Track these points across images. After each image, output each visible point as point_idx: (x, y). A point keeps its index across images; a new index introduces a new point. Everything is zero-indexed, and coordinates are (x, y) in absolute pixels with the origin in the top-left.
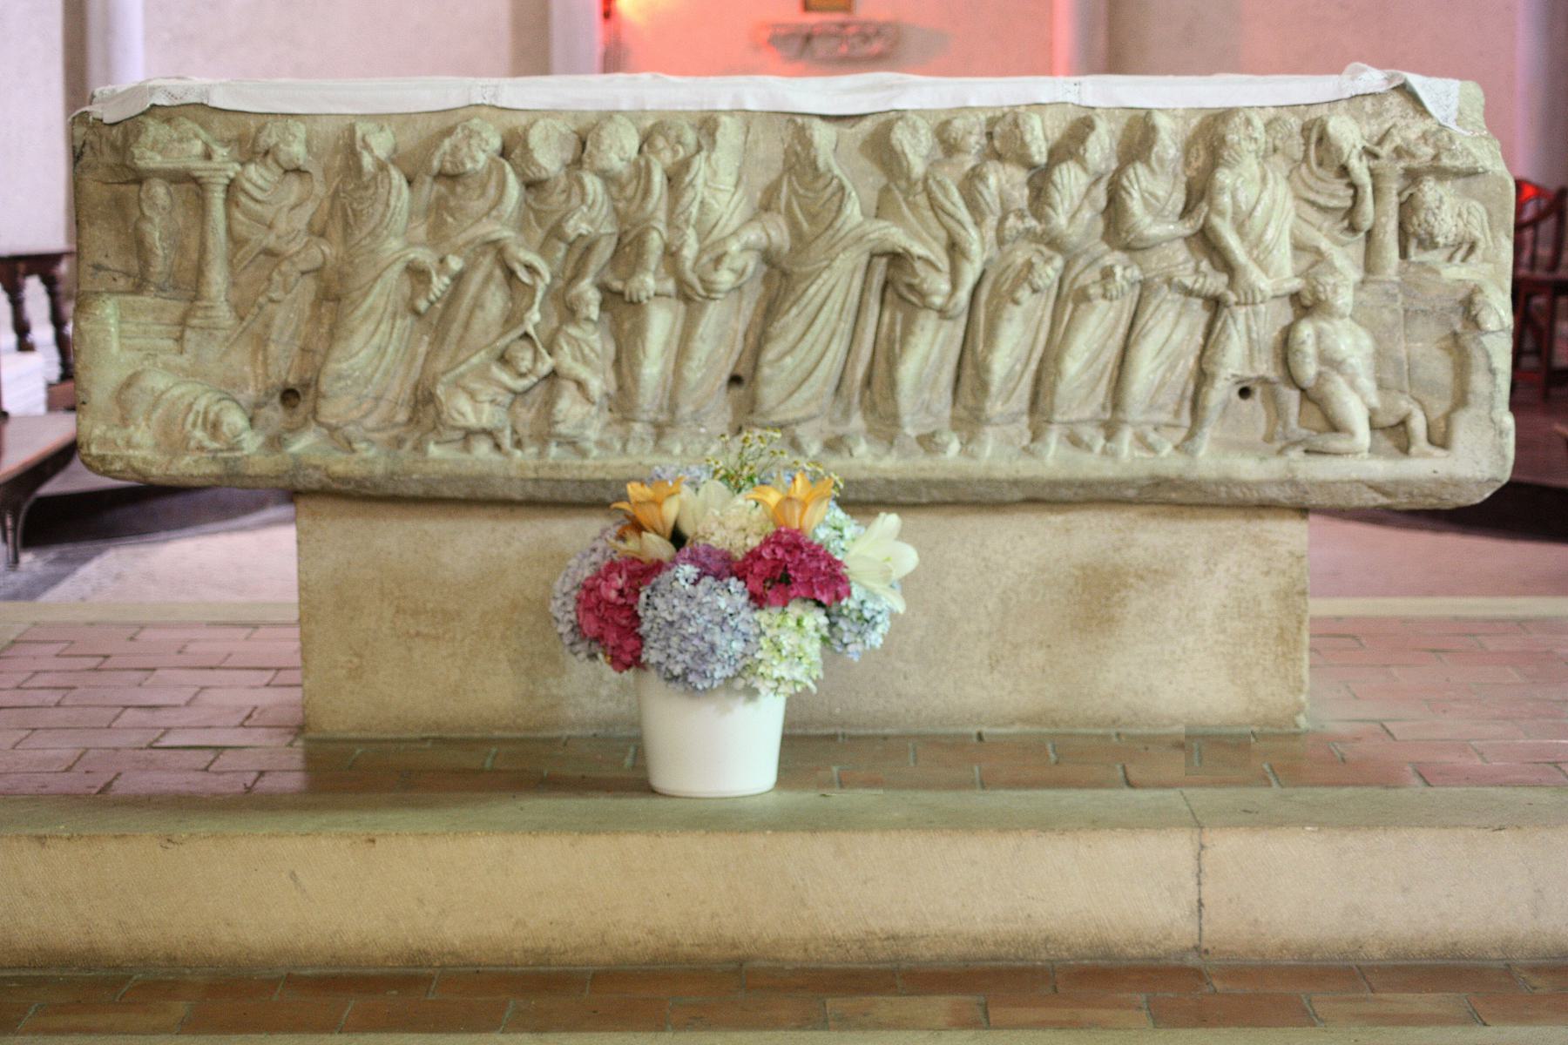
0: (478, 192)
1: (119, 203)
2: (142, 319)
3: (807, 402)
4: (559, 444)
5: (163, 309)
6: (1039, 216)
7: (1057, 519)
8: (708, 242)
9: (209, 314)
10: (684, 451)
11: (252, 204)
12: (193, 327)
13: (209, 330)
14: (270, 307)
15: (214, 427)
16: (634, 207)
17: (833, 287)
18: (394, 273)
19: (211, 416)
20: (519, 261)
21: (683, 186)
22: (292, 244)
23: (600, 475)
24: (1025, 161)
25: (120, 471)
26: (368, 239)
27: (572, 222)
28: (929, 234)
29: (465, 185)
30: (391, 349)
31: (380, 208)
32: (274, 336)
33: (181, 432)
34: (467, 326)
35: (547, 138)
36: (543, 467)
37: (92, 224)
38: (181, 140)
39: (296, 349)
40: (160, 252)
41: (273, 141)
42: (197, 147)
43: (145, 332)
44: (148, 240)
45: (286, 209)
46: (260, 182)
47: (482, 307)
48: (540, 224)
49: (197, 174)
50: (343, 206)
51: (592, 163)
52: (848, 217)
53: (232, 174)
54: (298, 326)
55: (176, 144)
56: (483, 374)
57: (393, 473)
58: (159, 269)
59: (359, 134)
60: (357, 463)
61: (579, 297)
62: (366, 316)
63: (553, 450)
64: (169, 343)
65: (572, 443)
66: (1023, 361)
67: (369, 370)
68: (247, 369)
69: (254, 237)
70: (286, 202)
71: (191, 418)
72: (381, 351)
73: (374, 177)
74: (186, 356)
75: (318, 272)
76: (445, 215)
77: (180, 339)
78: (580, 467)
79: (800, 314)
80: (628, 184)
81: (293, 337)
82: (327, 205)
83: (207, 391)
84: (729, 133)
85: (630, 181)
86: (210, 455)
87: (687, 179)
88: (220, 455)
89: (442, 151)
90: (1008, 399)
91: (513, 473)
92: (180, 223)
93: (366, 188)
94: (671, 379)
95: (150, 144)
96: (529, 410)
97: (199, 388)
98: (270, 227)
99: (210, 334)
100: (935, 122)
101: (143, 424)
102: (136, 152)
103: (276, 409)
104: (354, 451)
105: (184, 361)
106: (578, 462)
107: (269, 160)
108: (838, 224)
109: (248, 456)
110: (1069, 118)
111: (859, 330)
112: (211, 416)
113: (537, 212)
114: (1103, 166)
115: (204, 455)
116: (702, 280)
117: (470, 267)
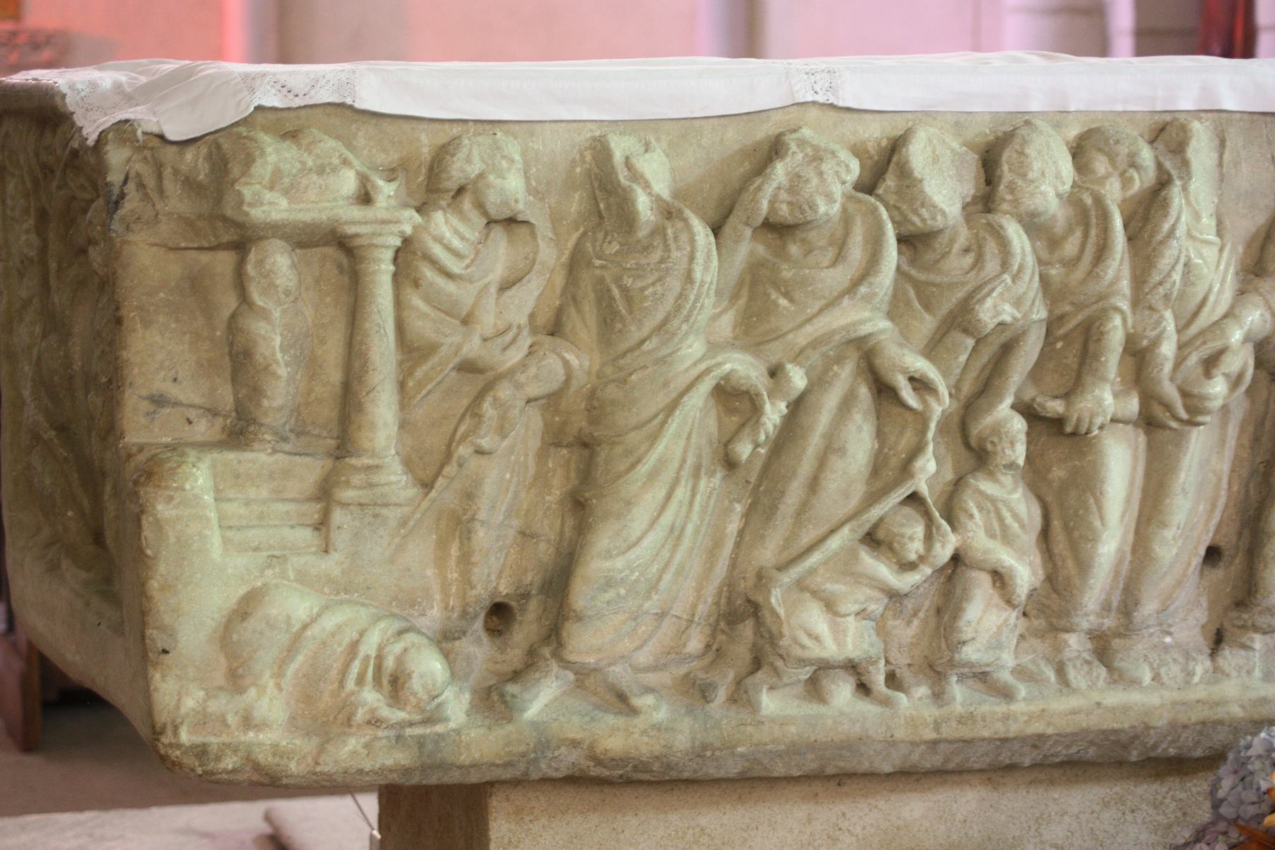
0: (831, 253)
1: (196, 285)
2: (252, 493)
4: (962, 678)
5: (286, 473)
8: (1193, 330)
9: (375, 479)
10: (1156, 677)
11: (441, 281)
12: (345, 505)
13: (372, 508)
14: (474, 463)
15: (396, 685)
16: (1079, 273)
18: (698, 399)
19: (390, 663)
20: (904, 371)
21: (1159, 237)
22: (509, 353)
23: (1037, 727)
25: (234, 771)
26: (655, 341)
27: (989, 303)
29: (803, 241)
30: (690, 529)
31: (674, 284)
32: (482, 515)
33: (334, 694)
34: (814, 485)
35: (936, 160)
36: (947, 720)
37: (147, 324)
38: (321, 171)
39: (512, 533)
40: (283, 371)
41: (474, 169)
42: (348, 182)
43: (261, 517)
44: (262, 351)
45: (493, 290)
46: (456, 243)
47: (842, 451)
48: (927, 307)
49: (351, 230)
50: (601, 280)
51: (1016, 202)
53: (408, 230)
54: (516, 495)
55: (315, 178)
56: (846, 567)
57: (705, 747)
58: (278, 402)
59: (618, 157)
60: (644, 732)
61: (997, 430)
62: (653, 475)
63: (958, 692)
64: (305, 535)
65: (982, 677)
67: (655, 568)
68: (430, 572)
69: (449, 340)
70: (491, 277)
71: (355, 668)
72: (676, 535)
73: (658, 231)
74: (335, 556)
75: (552, 401)
76: (774, 295)
77: (322, 525)
78: (1006, 718)
80: (1064, 238)
81: (508, 515)
82: (559, 280)
83: (378, 619)
84: (1201, 152)
85: (1070, 231)
86: (392, 733)
87: (1166, 227)
88: (409, 732)
89: (774, 185)
91: (900, 734)
92: (310, 320)
93: (647, 249)
94: (1128, 557)
95: (267, 178)
96: (909, 623)
97: (364, 614)
98: (467, 321)
99: (376, 516)
101: (271, 684)
102: (247, 192)
103: (478, 641)
104: (633, 711)
105: (332, 565)
106: (1001, 708)
107: (467, 203)
109: (458, 732)
112: (390, 663)
113: (917, 285)
115: (380, 733)
116: (1185, 394)
117: (818, 382)
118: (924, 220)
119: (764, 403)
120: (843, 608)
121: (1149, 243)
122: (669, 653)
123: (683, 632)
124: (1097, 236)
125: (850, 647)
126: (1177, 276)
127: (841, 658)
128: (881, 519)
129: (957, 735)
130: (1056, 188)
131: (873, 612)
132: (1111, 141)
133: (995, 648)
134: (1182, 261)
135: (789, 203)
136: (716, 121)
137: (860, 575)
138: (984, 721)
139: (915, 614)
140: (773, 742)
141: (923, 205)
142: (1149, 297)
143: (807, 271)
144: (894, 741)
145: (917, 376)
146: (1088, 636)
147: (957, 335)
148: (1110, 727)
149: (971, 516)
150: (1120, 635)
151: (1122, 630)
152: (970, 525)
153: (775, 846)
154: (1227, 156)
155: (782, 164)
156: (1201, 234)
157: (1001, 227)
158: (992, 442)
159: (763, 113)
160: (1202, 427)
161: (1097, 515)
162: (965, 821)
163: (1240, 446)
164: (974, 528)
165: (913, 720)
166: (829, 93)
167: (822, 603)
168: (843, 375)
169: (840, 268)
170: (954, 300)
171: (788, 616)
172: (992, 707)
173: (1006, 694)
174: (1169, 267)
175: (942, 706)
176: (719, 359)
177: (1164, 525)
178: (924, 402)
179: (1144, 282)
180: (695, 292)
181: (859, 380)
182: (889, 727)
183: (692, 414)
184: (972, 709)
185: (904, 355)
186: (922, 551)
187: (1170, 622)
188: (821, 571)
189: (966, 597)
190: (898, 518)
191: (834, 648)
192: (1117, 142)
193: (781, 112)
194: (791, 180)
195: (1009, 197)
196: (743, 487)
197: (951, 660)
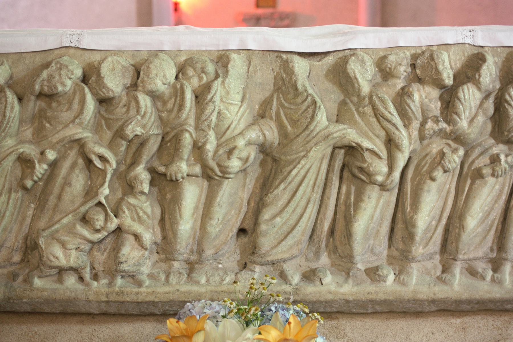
3: (291, 247)
6: (449, 121)
7: (457, 321)
8: (223, 139)
10: (208, 281)
16: (173, 116)
17: (309, 169)
20: (95, 154)
21: (206, 101)
24: (438, 84)
27: (130, 127)
28: (373, 133)
29: (57, 101)
30: (8, 213)
34: (59, 197)
47: (70, 185)
48: (109, 128)
51: (144, 87)
52: (319, 122)
56: (71, 230)
57: (9, 299)
61: (136, 178)
63: (119, 281)
66: (437, 218)
78: (137, 293)
79: (285, 189)
80: (168, 101)
85: (170, 98)
87: (209, 97)
89: (41, 79)
90: (427, 244)
91: (91, 298)
96: (103, 254)
100: (376, 57)
108: (311, 127)
110: (466, 54)
111: (325, 198)
114: (491, 86)
116: (219, 165)
118: (104, 93)
119: (36, 165)
120: (68, 247)
121: (202, 104)
122: (5, 262)
123: (10, 253)
124: (179, 101)
125: (72, 262)
126: (214, 118)
127: (68, 266)
128: (87, 211)
129: (116, 299)
130: (162, 81)
131: (83, 249)
132: (194, 62)
133: (137, 265)
134: (216, 110)
135: (48, 86)
136: (31, 54)
137: (75, 234)
138: (128, 294)
139: (105, 251)
140: (38, 298)
141: (103, 88)
142: (201, 125)
143: (56, 113)
144: (89, 300)
145: (101, 155)
146: (186, 263)
147: (119, 140)
148: (183, 300)
149: (124, 212)
150: (197, 263)
151: (198, 261)
152: (124, 215)
153: (66, 341)
154: (250, 68)
155: (46, 71)
156: (228, 100)
157: (137, 96)
158: (134, 183)
159: (51, 51)
160: (230, 179)
161: (178, 214)
162: (147, 336)
163: (255, 187)
164: (125, 217)
165: (97, 292)
166: (77, 43)
167: (61, 245)
168: (72, 155)
169: (69, 112)
170: (118, 126)
171: (46, 248)
172: (133, 289)
173: (139, 284)
174: (210, 114)
175: (110, 288)
176: (19, 147)
177: (211, 219)
178: (105, 166)
179: (200, 119)
180: (7, 120)
181: (79, 157)
182: (86, 295)
183: (7, 168)
184: (123, 289)
185: (94, 147)
186: (102, 225)
187: (221, 258)
188: (61, 232)
189: (122, 244)
190: (94, 212)
191: (65, 262)
192: (197, 62)
193: (58, 50)
194: (48, 77)
195: (141, 85)
196: (34, 198)
197: (116, 270)
